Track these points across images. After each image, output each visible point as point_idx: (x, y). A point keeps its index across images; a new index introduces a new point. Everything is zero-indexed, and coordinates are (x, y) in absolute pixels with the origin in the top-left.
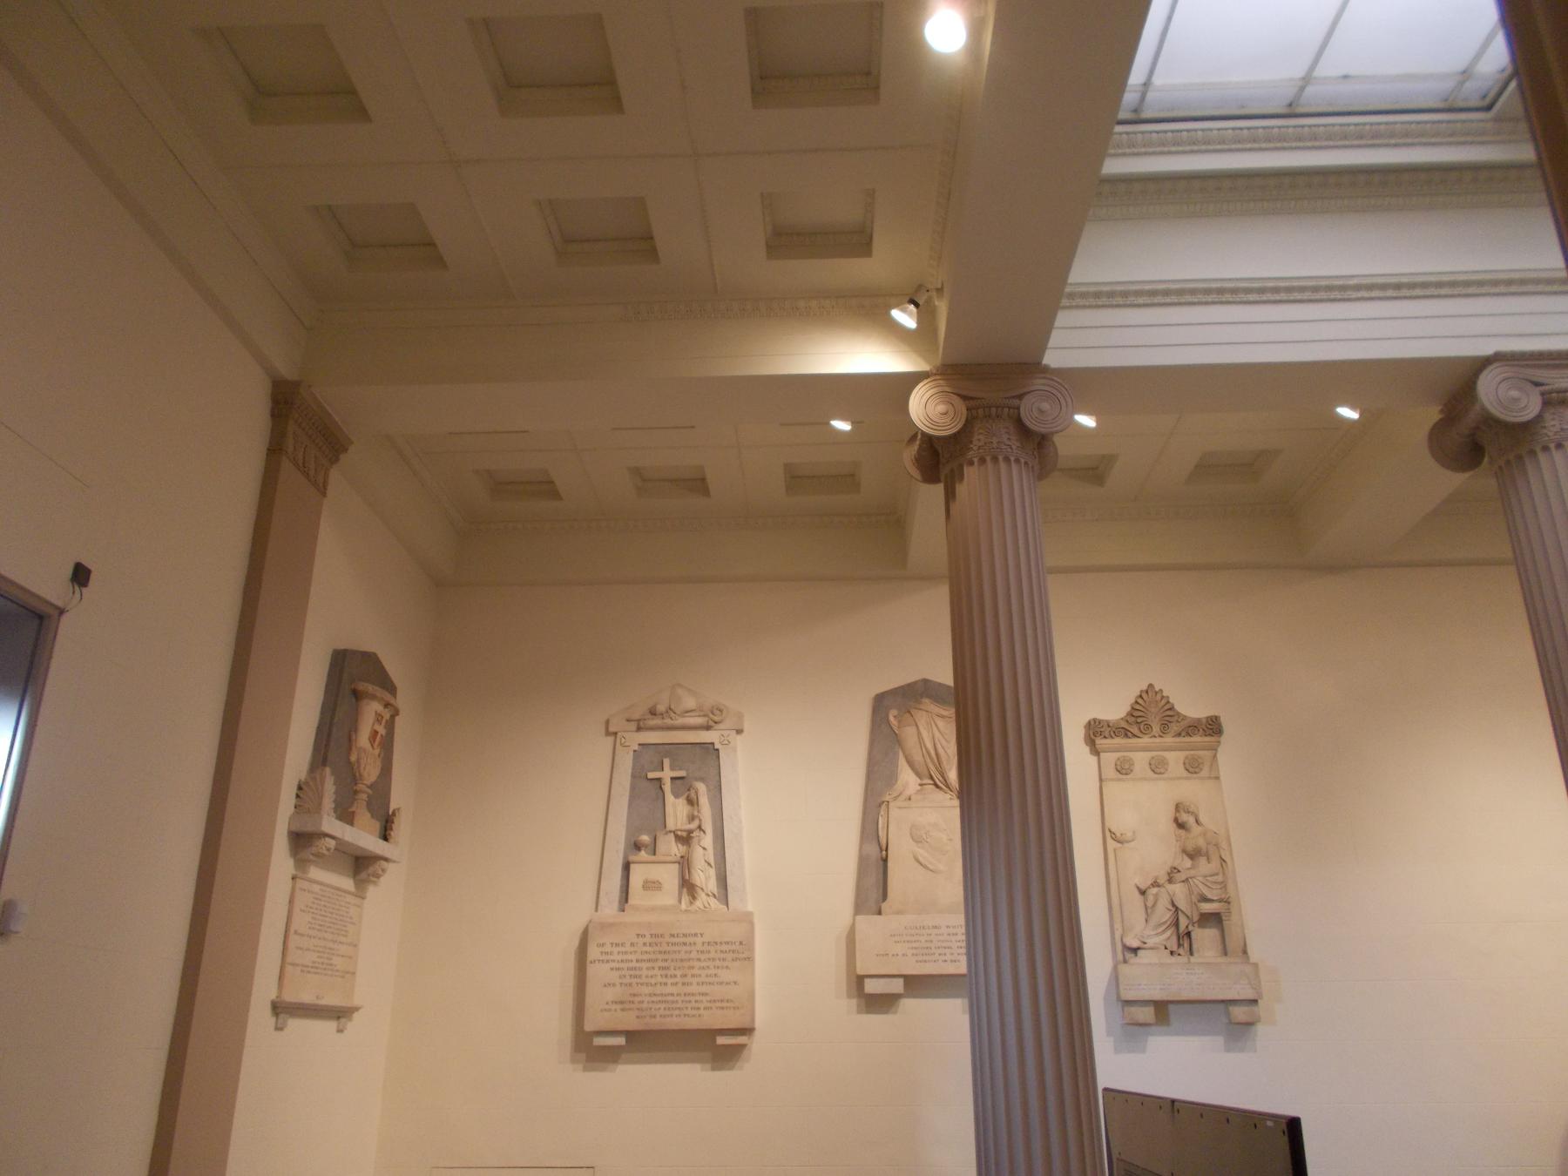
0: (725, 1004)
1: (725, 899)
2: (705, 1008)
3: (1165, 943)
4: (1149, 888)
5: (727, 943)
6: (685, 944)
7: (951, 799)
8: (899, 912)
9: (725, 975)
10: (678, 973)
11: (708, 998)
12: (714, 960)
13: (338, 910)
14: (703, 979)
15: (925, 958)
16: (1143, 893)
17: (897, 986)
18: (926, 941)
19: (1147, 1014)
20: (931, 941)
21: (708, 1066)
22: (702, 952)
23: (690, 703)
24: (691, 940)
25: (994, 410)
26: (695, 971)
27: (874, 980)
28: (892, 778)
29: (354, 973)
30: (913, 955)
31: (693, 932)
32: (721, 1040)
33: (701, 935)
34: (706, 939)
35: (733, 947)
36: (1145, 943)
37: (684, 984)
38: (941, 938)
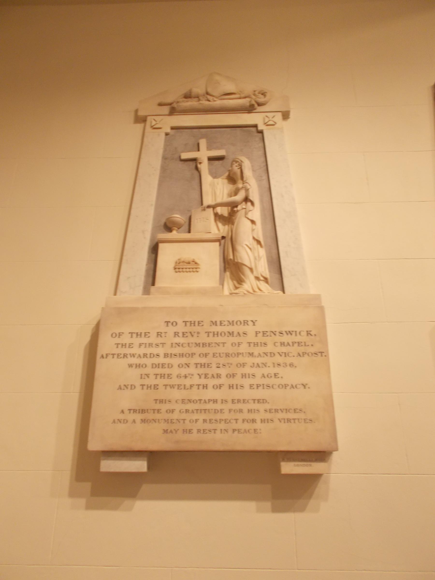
2: (262, 421)
5: (290, 333)
6: (231, 334)
10: (223, 372)
11: (267, 406)
14: (258, 380)
21: (268, 505)
23: (230, 87)
24: (241, 329)
26: (247, 370)
34: (259, 327)
35: (298, 339)
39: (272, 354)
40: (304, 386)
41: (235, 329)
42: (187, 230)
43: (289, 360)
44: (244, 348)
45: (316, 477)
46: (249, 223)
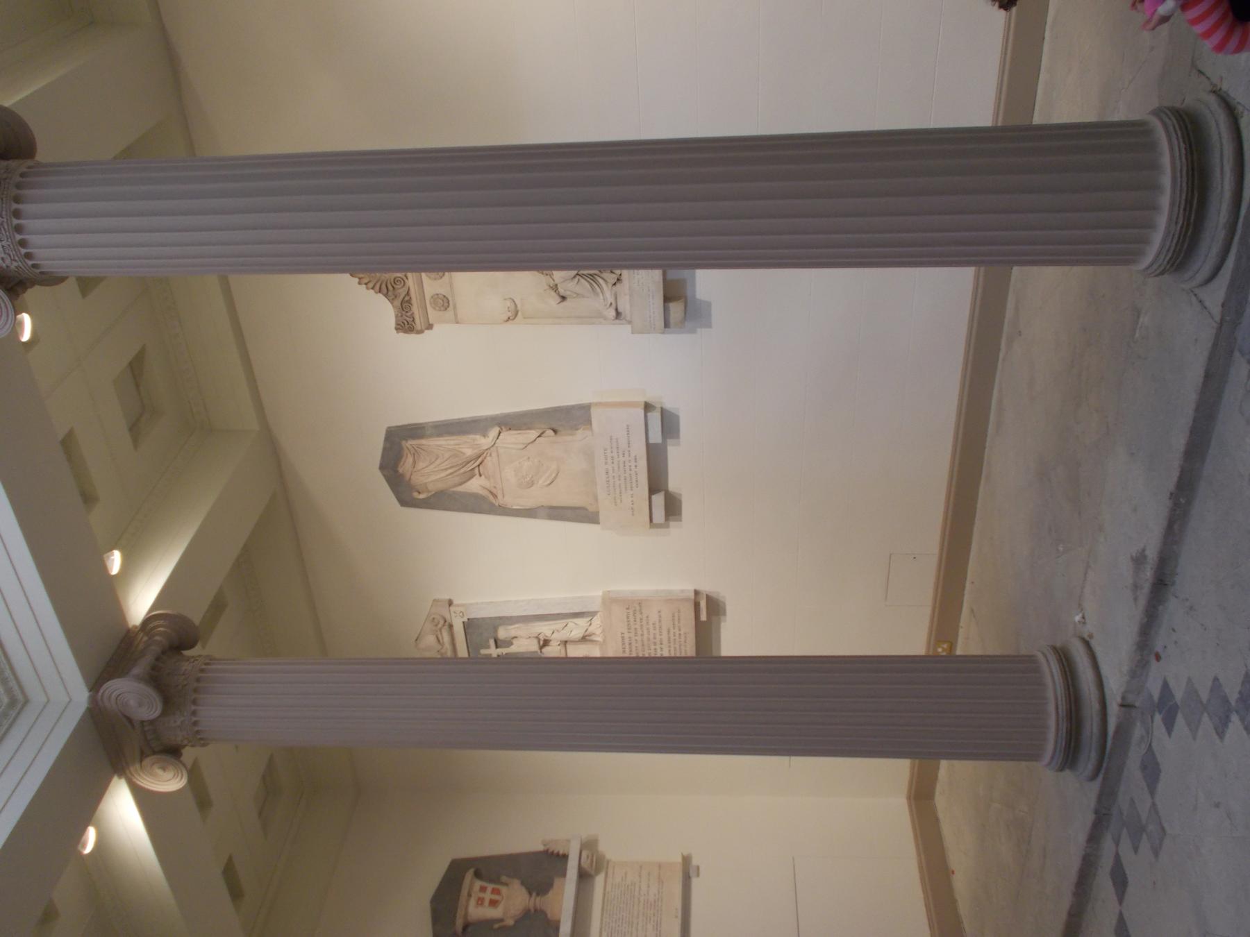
0: (676, 618)
1: (592, 614)
2: (680, 630)
3: (610, 285)
4: (558, 294)
5: (628, 618)
6: (630, 644)
7: (491, 455)
8: (596, 499)
9: (654, 617)
10: (653, 647)
11: (672, 629)
12: (642, 625)
13: (618, 898)
14: (657, 631)
15: (634, 480)
16: (563, 298)
17: (659, 499)
18: (619, 480)
19: (676, 309)
20: (619, 476)
21: (722, 618)
22: (636, 633)
23: (430, 640)
24: (627, 641)
25: (146, 729)
26: (652, 636)
27: (654, 516)
28: (475, 496)
29: (660, 866)
30: (632, 490)
31: (620, 639)
32: (703, 617)
33: (622, 634)
34: (625, 631)
35: (631, 613)
36: (611, 304)
37: (661, 644)
38: (616, 468)
39: (642, 625)
40: (659, 612)
41: (627, 641)
42: (660, 323)
43: (645, 619)
44: (639, 638)
45: (707, 595)
46: (554, 634)
